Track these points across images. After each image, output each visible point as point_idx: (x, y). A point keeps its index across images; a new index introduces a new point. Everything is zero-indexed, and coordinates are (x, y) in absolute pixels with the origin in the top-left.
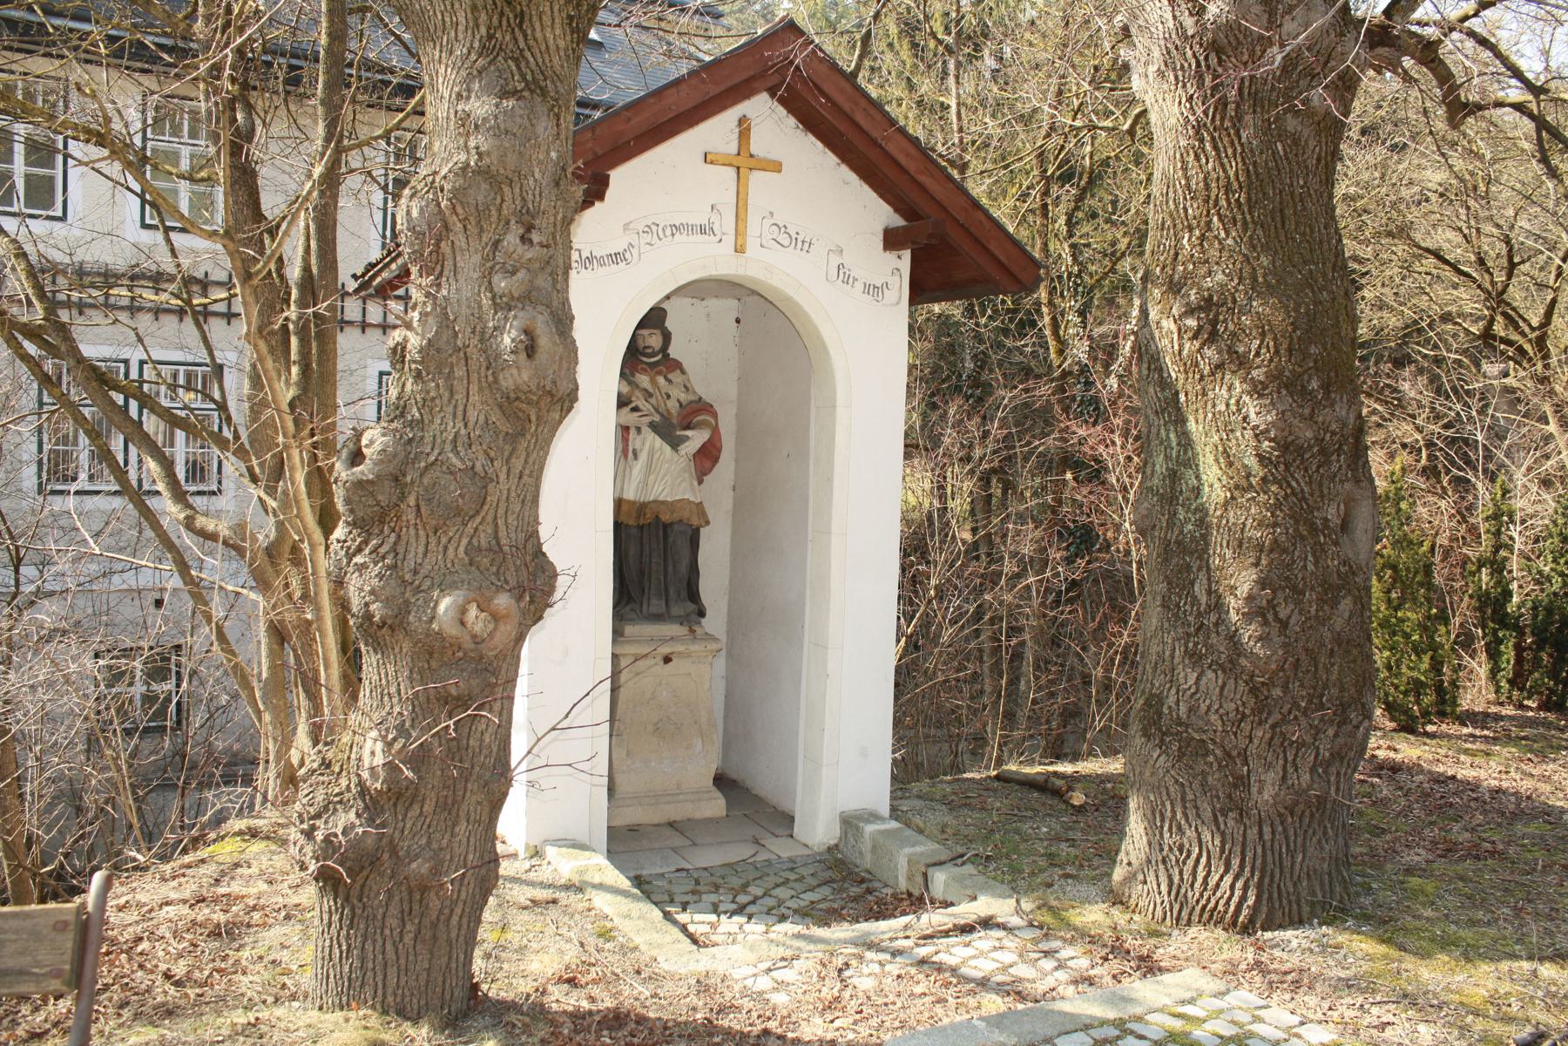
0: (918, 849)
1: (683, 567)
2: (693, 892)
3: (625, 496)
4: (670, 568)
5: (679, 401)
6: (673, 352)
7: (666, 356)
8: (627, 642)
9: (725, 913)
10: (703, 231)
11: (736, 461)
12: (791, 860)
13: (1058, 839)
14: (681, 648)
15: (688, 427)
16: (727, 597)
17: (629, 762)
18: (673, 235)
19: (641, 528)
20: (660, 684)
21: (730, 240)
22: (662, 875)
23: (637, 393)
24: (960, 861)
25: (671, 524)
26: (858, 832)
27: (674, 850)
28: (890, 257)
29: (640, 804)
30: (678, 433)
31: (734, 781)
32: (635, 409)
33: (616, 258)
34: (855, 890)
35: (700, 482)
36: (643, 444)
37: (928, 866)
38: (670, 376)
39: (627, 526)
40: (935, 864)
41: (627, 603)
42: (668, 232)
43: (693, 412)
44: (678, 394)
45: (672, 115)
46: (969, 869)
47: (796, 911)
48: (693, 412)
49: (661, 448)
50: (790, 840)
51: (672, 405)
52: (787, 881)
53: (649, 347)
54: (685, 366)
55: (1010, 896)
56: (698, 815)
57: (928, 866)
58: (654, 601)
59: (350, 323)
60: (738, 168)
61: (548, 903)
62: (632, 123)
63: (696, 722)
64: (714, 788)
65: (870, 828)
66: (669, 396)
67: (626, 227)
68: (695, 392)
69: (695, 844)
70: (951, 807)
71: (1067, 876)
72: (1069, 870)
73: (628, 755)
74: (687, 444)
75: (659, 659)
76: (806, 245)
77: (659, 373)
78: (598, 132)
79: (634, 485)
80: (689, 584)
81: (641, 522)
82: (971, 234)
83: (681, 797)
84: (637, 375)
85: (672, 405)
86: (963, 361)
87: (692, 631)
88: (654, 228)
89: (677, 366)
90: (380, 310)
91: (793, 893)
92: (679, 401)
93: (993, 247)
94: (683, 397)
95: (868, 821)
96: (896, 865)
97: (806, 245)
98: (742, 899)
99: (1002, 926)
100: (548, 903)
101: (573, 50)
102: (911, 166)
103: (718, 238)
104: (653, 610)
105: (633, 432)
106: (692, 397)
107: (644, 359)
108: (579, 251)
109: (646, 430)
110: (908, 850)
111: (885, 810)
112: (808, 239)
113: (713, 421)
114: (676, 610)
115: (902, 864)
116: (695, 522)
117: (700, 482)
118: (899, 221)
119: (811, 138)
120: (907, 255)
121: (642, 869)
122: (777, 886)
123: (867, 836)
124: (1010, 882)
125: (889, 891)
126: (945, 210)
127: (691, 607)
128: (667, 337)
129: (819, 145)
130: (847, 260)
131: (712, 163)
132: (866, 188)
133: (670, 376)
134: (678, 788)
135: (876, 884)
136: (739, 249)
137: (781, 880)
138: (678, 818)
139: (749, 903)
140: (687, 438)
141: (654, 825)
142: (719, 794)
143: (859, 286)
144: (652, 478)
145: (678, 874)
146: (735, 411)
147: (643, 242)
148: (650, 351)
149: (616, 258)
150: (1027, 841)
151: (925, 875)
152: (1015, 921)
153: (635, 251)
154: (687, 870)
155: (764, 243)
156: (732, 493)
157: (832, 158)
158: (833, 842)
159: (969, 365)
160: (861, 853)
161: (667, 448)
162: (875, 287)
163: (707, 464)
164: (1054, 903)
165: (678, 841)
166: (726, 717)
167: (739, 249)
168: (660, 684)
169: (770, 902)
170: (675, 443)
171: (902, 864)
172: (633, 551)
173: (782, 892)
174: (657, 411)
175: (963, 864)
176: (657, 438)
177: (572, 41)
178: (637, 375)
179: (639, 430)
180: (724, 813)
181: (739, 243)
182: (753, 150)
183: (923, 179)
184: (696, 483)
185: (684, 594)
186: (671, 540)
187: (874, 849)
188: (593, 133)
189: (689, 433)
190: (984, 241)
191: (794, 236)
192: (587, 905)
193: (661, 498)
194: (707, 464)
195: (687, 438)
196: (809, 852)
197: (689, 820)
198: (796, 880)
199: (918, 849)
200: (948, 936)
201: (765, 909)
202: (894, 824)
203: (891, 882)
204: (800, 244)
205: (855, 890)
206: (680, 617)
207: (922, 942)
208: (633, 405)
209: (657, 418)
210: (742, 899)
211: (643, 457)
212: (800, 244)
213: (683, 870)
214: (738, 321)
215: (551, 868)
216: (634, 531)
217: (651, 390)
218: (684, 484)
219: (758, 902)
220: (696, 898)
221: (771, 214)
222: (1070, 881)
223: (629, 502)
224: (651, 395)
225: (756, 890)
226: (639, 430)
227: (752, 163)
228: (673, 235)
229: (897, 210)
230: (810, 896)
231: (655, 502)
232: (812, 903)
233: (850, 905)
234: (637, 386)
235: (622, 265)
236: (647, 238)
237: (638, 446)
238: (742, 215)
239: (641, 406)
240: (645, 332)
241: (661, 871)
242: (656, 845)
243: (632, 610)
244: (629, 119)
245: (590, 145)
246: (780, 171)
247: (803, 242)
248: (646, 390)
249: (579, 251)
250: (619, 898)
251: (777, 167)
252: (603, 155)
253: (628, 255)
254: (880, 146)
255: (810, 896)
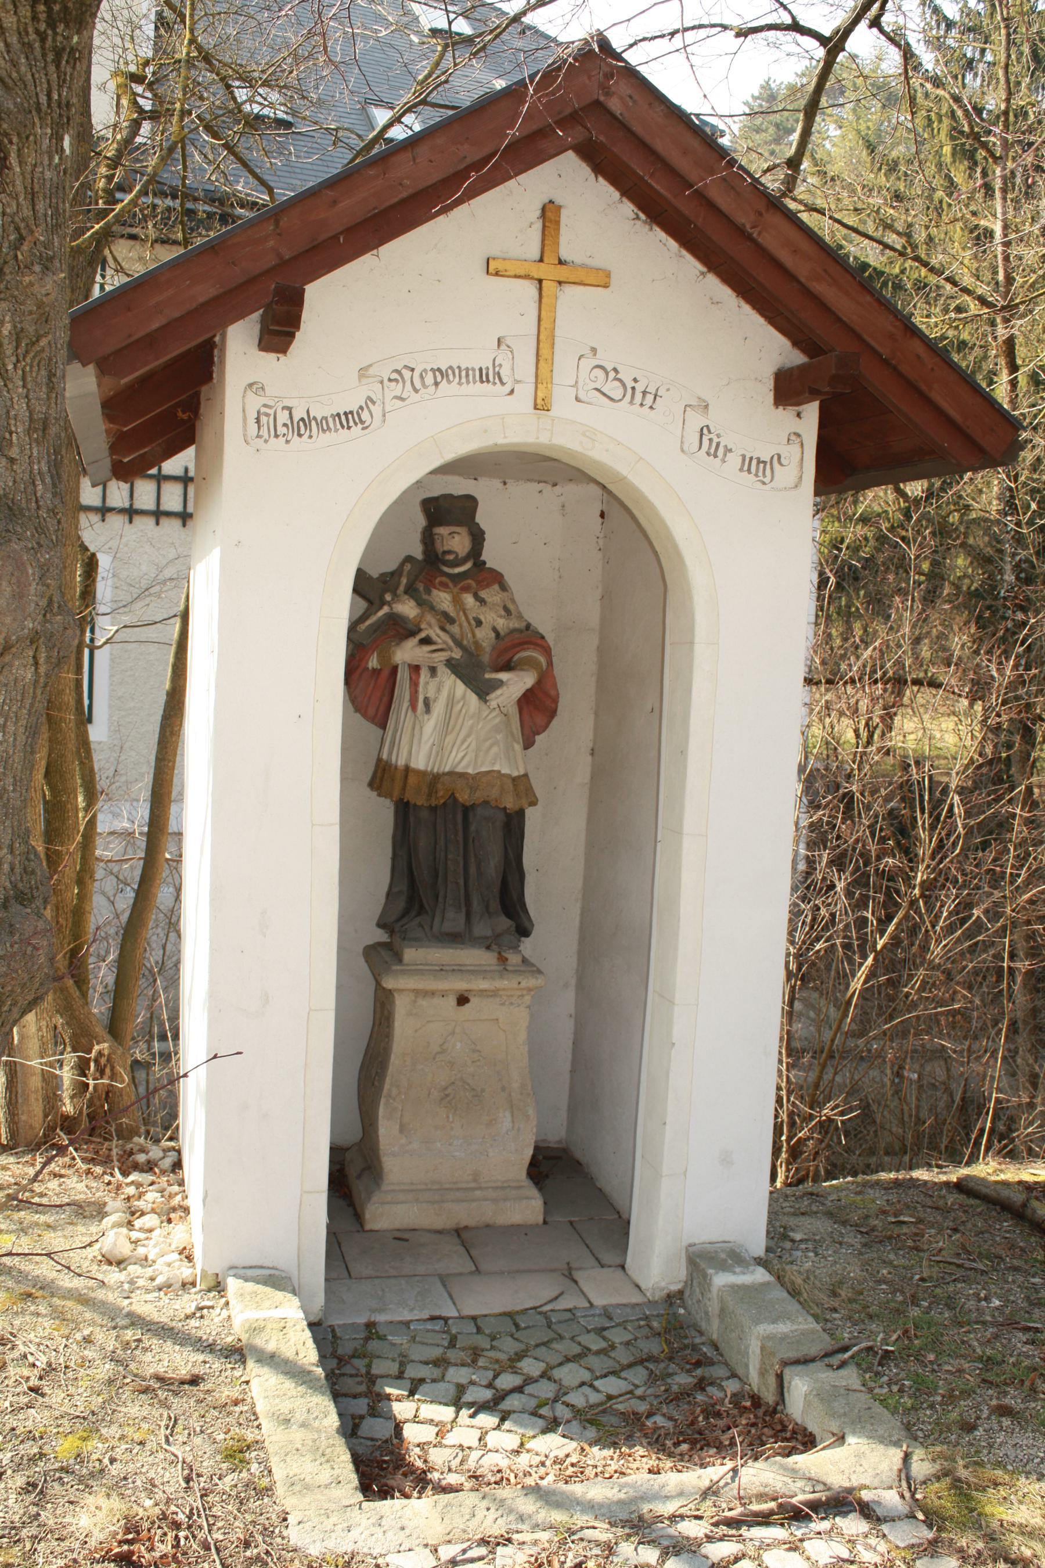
0: (783, 1328)
1: (493, 866)
2: (436, 1363)
3: (413, 765)
4: (473, 870)
5: (495, 630)
6: (491, 556)
7: (480, 565)
8: (404, 972)
9: (470, 1405)
10: (483, 377)
11: (596, 714)
12: (607, 1313)
13: (1012, 1323)
14: (484, 985)
15: (507, 667)
16: (579, 905)
17: (403, 1141)
18: (436, 384)
19: (433, 809)
20: (453, 1033)
21: (526, 392)
22: (407, 1324)
23: (429, 617)
24: (836, 1360)
25: (473, 806)
26: (706, 1282)
27: (444, 1280)
28: (785, 416)
29: (417, 1200)
30: (487, 676)
31: (579, 1163)
32: (426, 641)
33: (347, 419)
34: (682, 1380)
35: (528, 744)
36: (439, 690)
37: (785, 1363)
38: (483, 594)
39: (415, 805)
40: (797, 1362)
41: (419, 914)
42: (429, 379)
43: (514, 646)
44: (494, 619)
45: (404, 194)
46: (850, 1376)
47: (577, 1413)
48: (514, 646)
49: (464, 697)
50: (619, 1271)
51: (485, 635)
52: (586, 1352)
53: (449, 552)
54: (508, 578)
55: (897, 1444)
56: (502, 1220)
57: (785, 1363)
58: (450, 914)
59: (168, 514)
60: (540, 281)
61: (183, 1383)
62: (341, 206)
63: (503, 1089)
64: (527, 1183)
65: (721, 1280)
66: (479, 623)
67: (363, 372)
68: (520, 617)
69: (478, 1271)
70: (872, 1238)
71: (1004, 1411)
72: (1013, 1399)
73: (401, 1131)
74: (499, 692)
75: (452, 1001)
76: (649, 399)
77: (466, 589)
78: (284, 222)
79: (425, 749)
80: (504, 883)
81: (434, 803)
82: (900, 375)
83: (478, 1193)
84: (435, 592)
85: (485, 635)
86: (1001, 572)
87: (502, 960)
88: (407, 374)
89: (497, 579)
90: (126, 493)
91: (586, 1376)
92: (495, 630)
93: (937, 396)
94: (501, 623)
95: (723, 1266)
96: (747, 1347)
97: (649, 399)
98: (507, 1381)
99: (866, 1511)
100: (183, 1383)
101: (42, 37)
102: (802, 269)
103: (507, 389)
104: (448, 927)
105: (424, 675)
106: (514, 624)
107: (446, 569)
108: (290, 409)
109: (444, 672)
110: (765, 1329)
111: (757, 1243)
112: (652, 389)
113: (542, 660)
114: (481, 929)
115: (754, 1348)
116: (510, 803)
117: (528, 744)
118: (798, 358)
119: (660, 234)
120: (812, 411)
121: (381, 1310)
122: (568, 1360)
123: (714, 1290)
124: (907, 1411)
125: (732, 1386)
126: (858, 337)
127: (504, 923)
128: (478, 537)
129: (673, 244)
130: (715, 419)
131: (497, 274)
132: (747, 308)
133: (483, 594)
134: (475, 1180)
135: (718, 1371)
136: (541, 406)
137: (577, 1350)
138: (471, 1222)
139: (513, 1391)
140: (500, 683)
141: (429, 1231)
142: (534, 1192)
143: (734, 461)
144: (449, 739)
145: (429, 1326)
146: (596, 642)
147: (389, 395)
148: (451, 557)
149: (347, 419)
150: (961, 1325)
151: (780, 1377)
152: (891, 1499)
153: (376, 410)
154: (446, 1320)
155: (582, 396)
156: (589, 758)
157: (692, 265)
158: (675, 1287)
159: (1010, 577)
160: (707, 1313)
161: (473, 698)
162: (759, 461)
163: (540, 719)
164: (963, 1473)
165: (457, 1262)
166: (573, 1071)
167: (541, 406)
168: (453, 1033)
169: (545, 1390)
170: (483, 690)
171: (754, 1348)
172: (423, 842)
173: (571, 1375)
174: (459, 644)
175: (843, 1365)
176: (459, 683)
177: (35, 18)
178: (435, 592)
179: (433, 670)
180: (540, 1219)
181: (540, 395)
182: (565, 253)
183: (821, 288)
184: (518, 747)
185: (495, 905)
186: (473, 828)
187: (723, 1312)
188: (277, 223)
189: (503, 676)
190: (923, 387)
191: (630, 384)
192: (235, 1394)
193: (460, 769)
194: (540, 719)
195: (500, 683)
196: (637, 1298)
197: (488, 1226)
198: (598, 1353)
199: (783, 1328)
200: (767, 1524)
201: (533, 1403)
202: (760, 1275)
203: (740, 1372)
204: (639, 396)
205: (682, 1380)
206: (486, 938)
207: (723, 1530)
208: (423, 635)
209: (457, 654)
210: (507, 1381)
211: (439, 708)
212: (639, 396)
213: (439, 1318)
214: (602, 515)
215: (225, 1313)
216: (425, 814)
217: (453, 614)
218: (495, 749)
219: (528, 1389)
220: (436, 1372)
221: (594, 350)
222: (1006, 1422)
223: (418, 772)
224: (452, 621)
225: (531, 1366)
226: (433, 670)
227: (562, 273)
228: (436, 384)
229: (796, 344)
230: (611, 1385)
231: (451, 774)
232: (610, 1397)
233: (665, 1409)
234: (432, 608)
235: (356, 430)
236: (397, 389)
237: (431, 694)
238: (545, 352)
239: (434, 638)
240: (442, 531)
241: (407, 1316)
242: (421, 1269)
243: (421, 925)
244: (335, 202)
245: (271, 243)
246: (606, 286)
247: (644, 393)
248: (445, 615)
249: (290, 409)
250: (289, 1384)
251: (602, 279)
252: (295, 258)
253: (365, 415)
254: (749, 238)
255: (611, 1385)
